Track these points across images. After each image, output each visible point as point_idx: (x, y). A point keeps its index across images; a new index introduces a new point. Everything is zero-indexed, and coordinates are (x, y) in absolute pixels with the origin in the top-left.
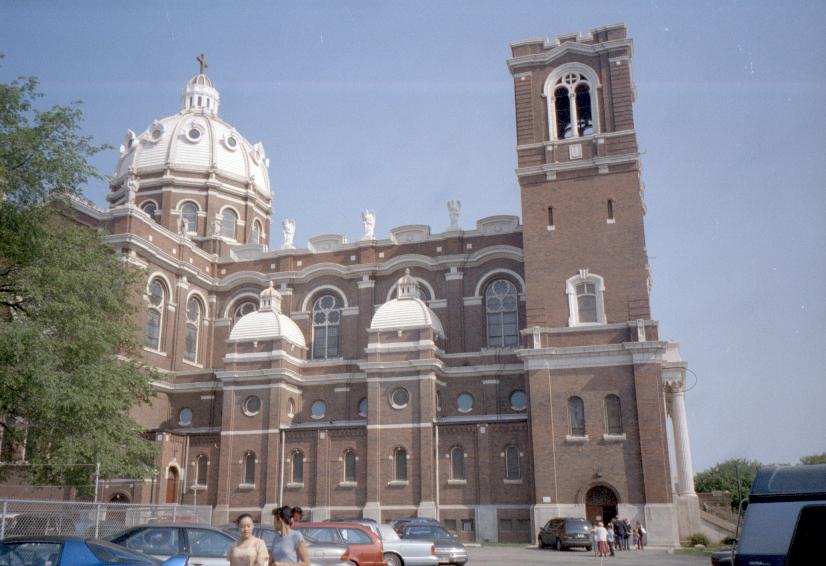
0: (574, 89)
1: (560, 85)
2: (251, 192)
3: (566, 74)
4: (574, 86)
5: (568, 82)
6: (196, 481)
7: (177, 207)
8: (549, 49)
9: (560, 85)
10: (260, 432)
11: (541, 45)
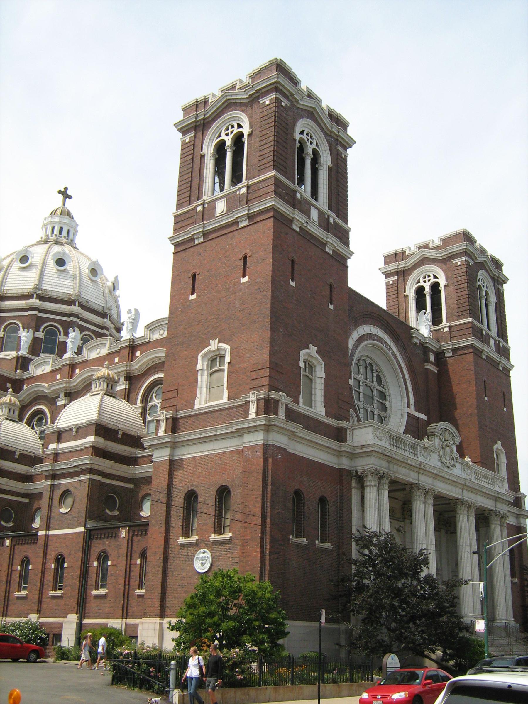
0: (428, 287)
1: (419, 284)
2: (107, 322)
3: (423, 276)
4: (231, 136)
5: (425, 282)
6: (279, 440)
7: (41, 330)
8: (409, 256)
9: (419, 284)
10: (51, 533)
11: (403, 253)
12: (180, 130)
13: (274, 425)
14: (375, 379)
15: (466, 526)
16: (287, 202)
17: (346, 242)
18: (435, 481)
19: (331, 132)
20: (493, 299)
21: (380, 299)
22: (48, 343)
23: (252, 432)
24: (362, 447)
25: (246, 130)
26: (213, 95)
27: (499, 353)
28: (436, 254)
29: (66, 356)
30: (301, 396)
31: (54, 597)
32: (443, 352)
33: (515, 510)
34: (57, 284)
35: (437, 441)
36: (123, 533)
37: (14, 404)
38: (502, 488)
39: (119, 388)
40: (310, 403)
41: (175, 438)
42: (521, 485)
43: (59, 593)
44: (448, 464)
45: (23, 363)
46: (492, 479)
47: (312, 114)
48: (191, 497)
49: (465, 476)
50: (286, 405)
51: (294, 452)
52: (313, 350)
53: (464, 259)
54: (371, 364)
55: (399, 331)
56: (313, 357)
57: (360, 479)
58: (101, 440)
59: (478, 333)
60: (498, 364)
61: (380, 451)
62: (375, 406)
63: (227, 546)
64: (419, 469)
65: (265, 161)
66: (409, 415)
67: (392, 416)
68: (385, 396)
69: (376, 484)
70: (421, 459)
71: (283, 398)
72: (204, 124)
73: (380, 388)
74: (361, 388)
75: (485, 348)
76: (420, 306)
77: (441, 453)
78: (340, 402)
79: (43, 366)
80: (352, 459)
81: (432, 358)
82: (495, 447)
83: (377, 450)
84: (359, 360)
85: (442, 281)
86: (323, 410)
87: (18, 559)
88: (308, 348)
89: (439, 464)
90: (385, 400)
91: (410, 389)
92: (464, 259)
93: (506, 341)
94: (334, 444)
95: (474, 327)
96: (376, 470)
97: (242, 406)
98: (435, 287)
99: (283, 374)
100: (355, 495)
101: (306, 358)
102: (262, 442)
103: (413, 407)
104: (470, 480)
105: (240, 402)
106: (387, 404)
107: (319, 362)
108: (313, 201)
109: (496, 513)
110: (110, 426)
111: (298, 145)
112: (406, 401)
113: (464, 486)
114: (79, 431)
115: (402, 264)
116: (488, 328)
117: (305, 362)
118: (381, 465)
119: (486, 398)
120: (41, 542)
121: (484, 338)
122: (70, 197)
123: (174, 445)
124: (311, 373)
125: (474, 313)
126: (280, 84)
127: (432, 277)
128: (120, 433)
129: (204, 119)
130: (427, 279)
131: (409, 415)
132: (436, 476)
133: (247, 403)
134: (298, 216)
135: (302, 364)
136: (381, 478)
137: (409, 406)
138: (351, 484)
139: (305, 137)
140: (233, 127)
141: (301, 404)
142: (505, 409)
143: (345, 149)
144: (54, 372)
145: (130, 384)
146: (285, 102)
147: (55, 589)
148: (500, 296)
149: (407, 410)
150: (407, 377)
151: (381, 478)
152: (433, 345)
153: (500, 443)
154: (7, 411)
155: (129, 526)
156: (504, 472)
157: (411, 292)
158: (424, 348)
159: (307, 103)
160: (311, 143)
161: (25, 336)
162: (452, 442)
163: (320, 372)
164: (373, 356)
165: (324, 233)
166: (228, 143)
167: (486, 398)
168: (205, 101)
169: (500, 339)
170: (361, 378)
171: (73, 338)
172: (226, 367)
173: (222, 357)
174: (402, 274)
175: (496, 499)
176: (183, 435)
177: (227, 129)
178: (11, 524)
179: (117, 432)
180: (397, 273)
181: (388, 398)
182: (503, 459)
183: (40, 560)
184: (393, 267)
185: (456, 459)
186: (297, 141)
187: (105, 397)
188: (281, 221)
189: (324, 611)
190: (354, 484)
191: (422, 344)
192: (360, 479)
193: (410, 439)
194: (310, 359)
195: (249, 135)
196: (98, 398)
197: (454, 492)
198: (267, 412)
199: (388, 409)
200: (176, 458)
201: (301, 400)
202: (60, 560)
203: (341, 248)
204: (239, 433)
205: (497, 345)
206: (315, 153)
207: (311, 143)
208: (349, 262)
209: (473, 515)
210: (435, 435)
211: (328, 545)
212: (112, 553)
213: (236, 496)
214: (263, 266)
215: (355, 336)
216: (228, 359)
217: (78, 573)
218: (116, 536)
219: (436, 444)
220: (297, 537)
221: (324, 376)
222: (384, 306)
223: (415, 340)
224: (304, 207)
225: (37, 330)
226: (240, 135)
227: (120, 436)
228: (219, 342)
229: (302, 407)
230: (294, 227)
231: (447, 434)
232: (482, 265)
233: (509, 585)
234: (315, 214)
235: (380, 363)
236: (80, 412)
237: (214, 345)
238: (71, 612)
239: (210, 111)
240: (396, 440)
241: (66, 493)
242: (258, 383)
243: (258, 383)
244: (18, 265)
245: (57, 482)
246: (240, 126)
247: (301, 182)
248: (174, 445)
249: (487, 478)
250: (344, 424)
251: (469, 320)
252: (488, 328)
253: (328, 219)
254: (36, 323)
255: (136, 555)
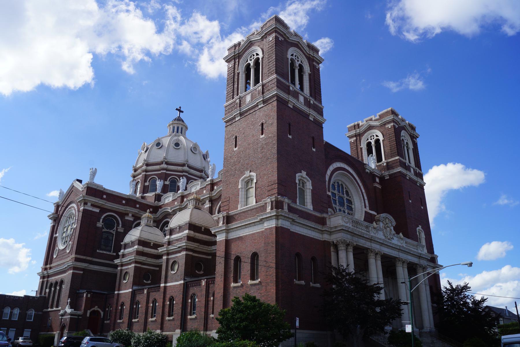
4: (253, 60)
6: (286, 224)
8: (361, 126)
12: (226, 61)
13: (281, 215)
14: (345, 193)
15: (402, 272)
16: (285, 92)
17: (322, 115)
18: (381, 247)
19: (310, 55)
20: (411, 146)
21: (347, 149)
22: (172, 187)
23: (269, 220)
24: (336, 227)
25: (260, 56)
26: (243, 41)
27: (417, 176)
28: (377, 123)
29: (179, 192)
30: (298, 199)
31: (169, 320)
32: (384, 177)
33: (432, 264)
34: (177, 157)
35: (381, 224)
36: (203, 283)
37: (151, 218)
38: (425, 251)
39: (206, 207)
40: (303, 202)
41: (228, 227)
42: (435, 250)
43: (171, 318)
44: (389, 237)
45: (158, 198)
46: (417, 246)
47: (297, 45)
48: (238, 259)
49: (400, 244)
50: (288, 205)
51: (295, 231)
52: (304, 174)
53: (392, 124)
54: (342, 185)
55: (358, 165)
56: (304, 178)
57: (336, 247)
58: (192, 232)
59: (403, 165)
60: (417, 182)
61: (346, 229)
62: (346, 207)
63: (258, 286)
64: (371, 240)
65: (271, 71)
66: (366, 212)
67: (356, 213)
68: (351, 202)
69: (345, 248)
70: (372, 234)
71: (286, 200)
72: (239, 56)
73: (348, 198)
74: (337, 197)
75: (408, 173)
76: (370, 152)
77: (384, 231)
78: (323, 202)
79: (169, 198)
80: (330, 235)
81: (377, 180)
82: (418, 229)
83: (344, 228)
84: (335, 183)
85: (381, 138)
86: (312, 207)
87: (151, 300)
88: (301, 172)
89: (383, 237)
90: (352, 204)
91: (366, 198)
92: (392, 124)
93: (420, 169)
94: (319, 227)
95: (400, 161)
96: (344, 240)
97: (263, 206)
98: (377, 141)
99: (286, 186)
100: (333, 254)
101: (300, 178)
102: (274, 225)
103: (368, 208)
104: (403, 246)
105: (261, 203)
106: (353, 206)
107: (308, 180)
108: (301, 92)
109: (421, 266)
110: (197, 225)
111: (290, 62)
112: (363, 204)
113: (400, 250)
114: (181, 228)
115: (358, 131)
116: (409, 162)
117: (299, 181)
118: (348, 238)
119: (410, 201)
120: (162, 290)
121: (408, 168)
122: (182, 112)
123: (228, 231)
124: (303, 186)
125: (400, 153)
126: (278, 28)
127: (375, 136)
128: (203, 228)
129: (238, 53)
130: (372, 137)
131: (366, 212)
132: (382, 244)
133: (266, 204)
134: (291, 99)
135: (297, 181)
136: (348, 245)
137: (365, 207)
138: (330, 250)
139: (294, 57)
140: (254, 55)
141: (298, 204)
142: (422, 208)
143: (319, 64)
144: (174, 201)
145: (212, 204)
146: (281, 38)
147: (169, 316)
148: (415, 145)
149: (364, 209)
150: (363, 191)
151: (348, 245)
152: (378, 173)
153: (420, 226)
154: (146, 220)
155: (207, 279)
156: (424, 242)
157: (364, 146)
158: (372, 175)
159: (293, 39)
160: (298, 61)
161: (159, 184)
162: (390, 225)
163: (309, 186)
164: (343, 180)
165: (308, 109)
166: (252, 64)
167: (410, 201)
168: (239, 44)
169: (417, 168)
170: (336, 192)
171: (182, 182)
172: (254, 185)
173: (252, 180)
174: (359, 136)
175: (420, 257)
176: (233, 225)
177: (251, 57)
178: (149, 282)
179: (201, 228)
180: (356, 136)
181: (353, 203)
182: (423, 235)
183: (162, 300)
184: (353, 132)
185: (394, 234)
186: (289, 60)
187: (195, 209)
188: (281, 103)
189: (98, 251)
190: (332, 249)
191: (371, 173)
192: (336, 247)
193: (366, 224)
194: (302, 179)
195: (262, 58)
196: (191, 209)
197: (394, 253)
198: (277, 208)
199: (353, 209)
200: (229, 238)
201: (298, 201)
202: (172, 299)
203: (319, 118)
204: (262, 221)
205: (415, 172)
206: (301, 66)
207: (298, 61)
208: (324, 125)
209: (406, 266)
210: (380, 221)
211: (318, 285)
212: (199, 294)
213: (262, 258)
214: (272, 129)
215: (331, 168)
216: (255, 181)
217: (181, 306)
218: (200, 285)
219: (381, 226)
220: (299, 280)
221: (311, 188)
222: (349, 153)
223: (367, 170)
224: (296, 95)
225: (165, 180)
226: (258, 59)
227: (203, 230)
228: (250, 172)
229: (298, 205)
230: (289, 105)
231: (387, 220)
232: (403, 128)
233: (430, 307)
234: (301, 99)
235: (347, 184)
236: (181, 219)
237: (247, 174)
238: (177, 329)
239: (242, 48)
240: (356, 223)
241: (174, 263)
242: (271, 193)
243: (271, 193)
244: (155, 147)
245: (170, 257)
246: (257, 54)
247: (293, 82)
248: (228, 231)
249: (413, 245)
250: (325, 215)
251: (397, 158)
252: (409, 162)
253: (310, 101)
254: (163, 177)
255: (211, 295)
